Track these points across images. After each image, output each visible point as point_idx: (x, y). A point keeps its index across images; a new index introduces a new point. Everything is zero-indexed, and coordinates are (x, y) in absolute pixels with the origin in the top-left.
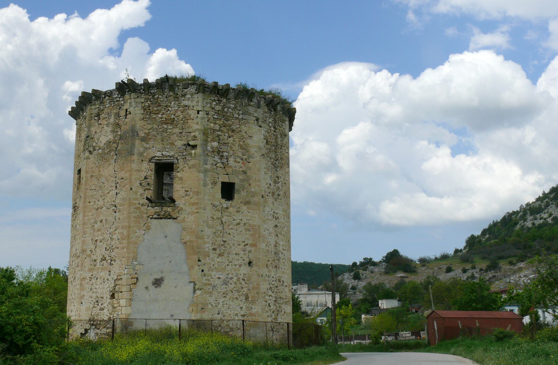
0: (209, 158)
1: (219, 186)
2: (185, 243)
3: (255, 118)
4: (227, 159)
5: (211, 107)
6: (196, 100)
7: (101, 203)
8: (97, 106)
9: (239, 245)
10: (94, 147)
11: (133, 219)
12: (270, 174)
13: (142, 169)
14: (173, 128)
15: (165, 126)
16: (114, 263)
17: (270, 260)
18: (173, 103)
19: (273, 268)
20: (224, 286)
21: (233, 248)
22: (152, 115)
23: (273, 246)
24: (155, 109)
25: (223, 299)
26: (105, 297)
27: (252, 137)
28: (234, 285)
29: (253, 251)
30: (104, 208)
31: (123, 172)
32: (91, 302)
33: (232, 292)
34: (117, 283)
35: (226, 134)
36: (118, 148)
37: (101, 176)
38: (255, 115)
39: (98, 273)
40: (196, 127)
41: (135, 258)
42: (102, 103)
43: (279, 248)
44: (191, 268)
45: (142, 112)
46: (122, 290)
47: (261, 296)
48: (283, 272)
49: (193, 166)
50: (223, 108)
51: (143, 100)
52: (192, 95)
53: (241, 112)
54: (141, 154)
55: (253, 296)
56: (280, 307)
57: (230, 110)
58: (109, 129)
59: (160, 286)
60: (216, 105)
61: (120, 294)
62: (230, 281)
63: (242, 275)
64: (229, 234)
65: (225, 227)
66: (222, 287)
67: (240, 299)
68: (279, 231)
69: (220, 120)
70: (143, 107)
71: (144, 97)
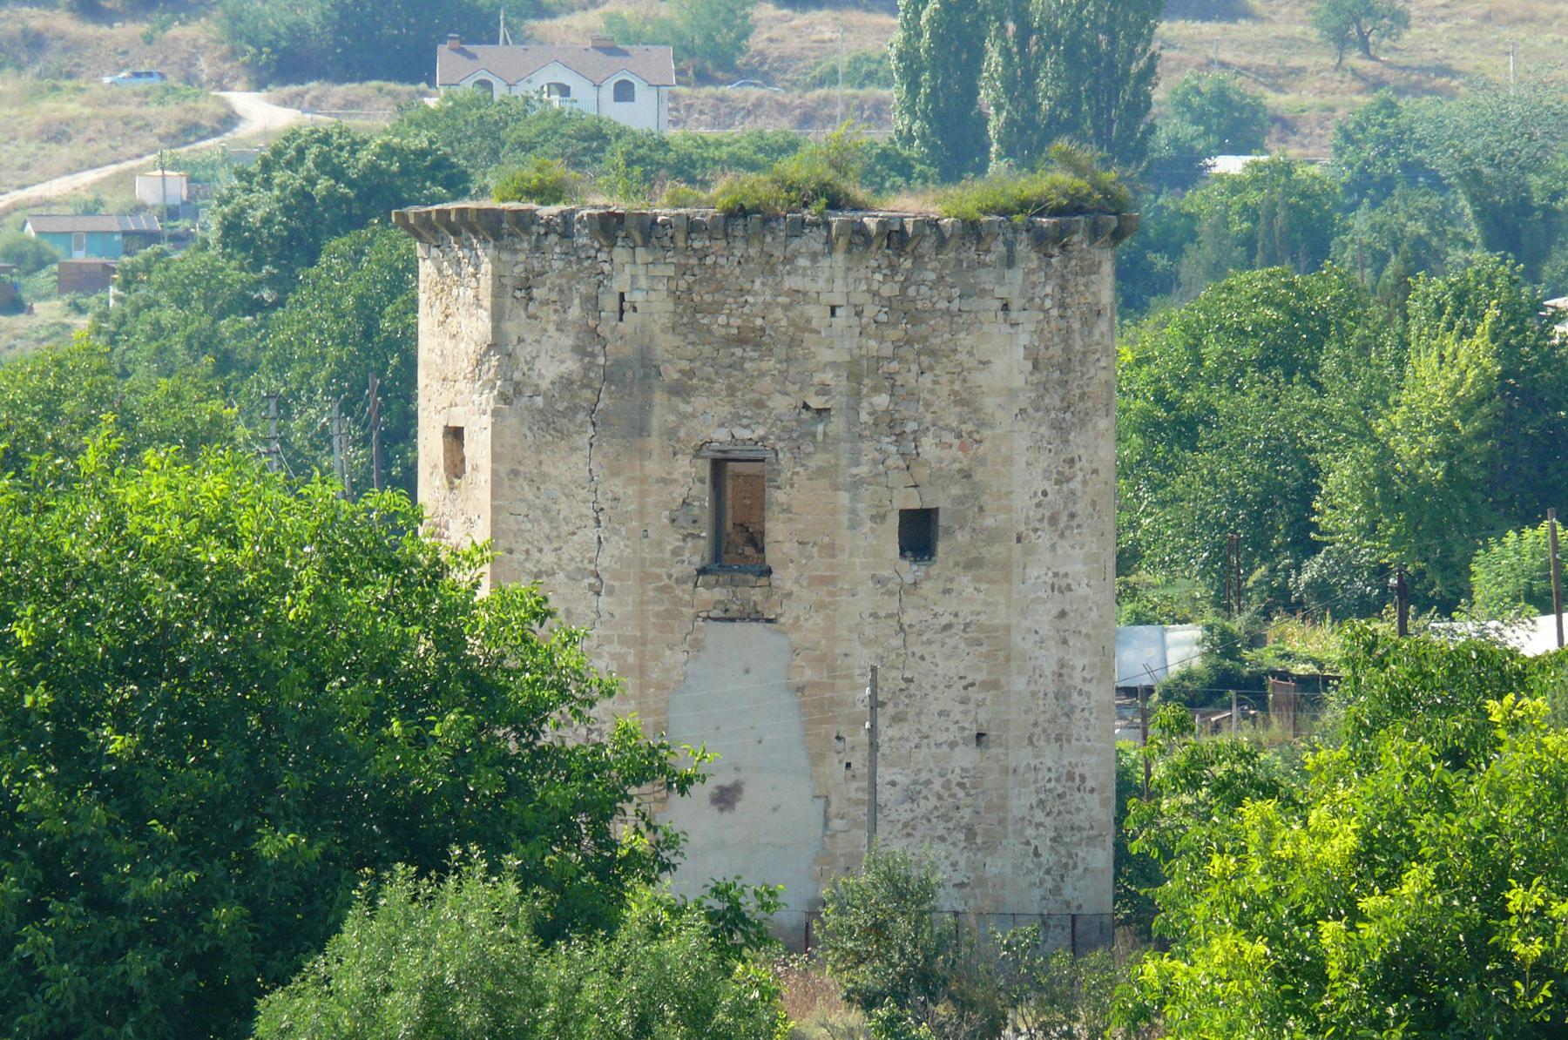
0: (865, 446)
1: (894, 521)
2: (800, 689)
3: (998, 304)
4: (915, 440)
5: (868, 291)
7: (548, 558)
8: (521, 257)
9: (949, 687)
10: (517, 384)
12: (1044, 461)
13: (676, 476)
14: (761, 358)
15: (738, 352)
17: (1042, 718)
19: (1048, 741)
20: (908, 805)
21: (930, 698)
22: (699, 316)
23: (1050, 677)
24: (708, 298)
25: (904, 842)
27: (989, 362)
28: (933, 802)
29: (988, 702)
30: (561, 576)
31: (617, 481)
33: (929, 820)
35: (915, 368)
36: (600, 406)
37: (545, 477)
38: (1000, 291)
40: (826, 355)
43: (1071, 677)
44: (817, 758)
45: (671, 306)
47: (1010, 828)
48: (1084, 750)
49: (821, 472)
50: (904, 289)
51: (670, 271)
52: (814, 257)
53: (956, 292)
54: (671, 433)
55: (986, 832)
56: (1070, 855)
57: (924, 289)
58: (567, 341)
59: (733, 807)
60: (883, 283)
62: (924, 792)
63: (958, 771)
64: (922, 658)
65: (911, 639)
66: (901, 808)
67: (950, 840)
68: (1073, 626)
69: (895, 325)
70: (671, 293)
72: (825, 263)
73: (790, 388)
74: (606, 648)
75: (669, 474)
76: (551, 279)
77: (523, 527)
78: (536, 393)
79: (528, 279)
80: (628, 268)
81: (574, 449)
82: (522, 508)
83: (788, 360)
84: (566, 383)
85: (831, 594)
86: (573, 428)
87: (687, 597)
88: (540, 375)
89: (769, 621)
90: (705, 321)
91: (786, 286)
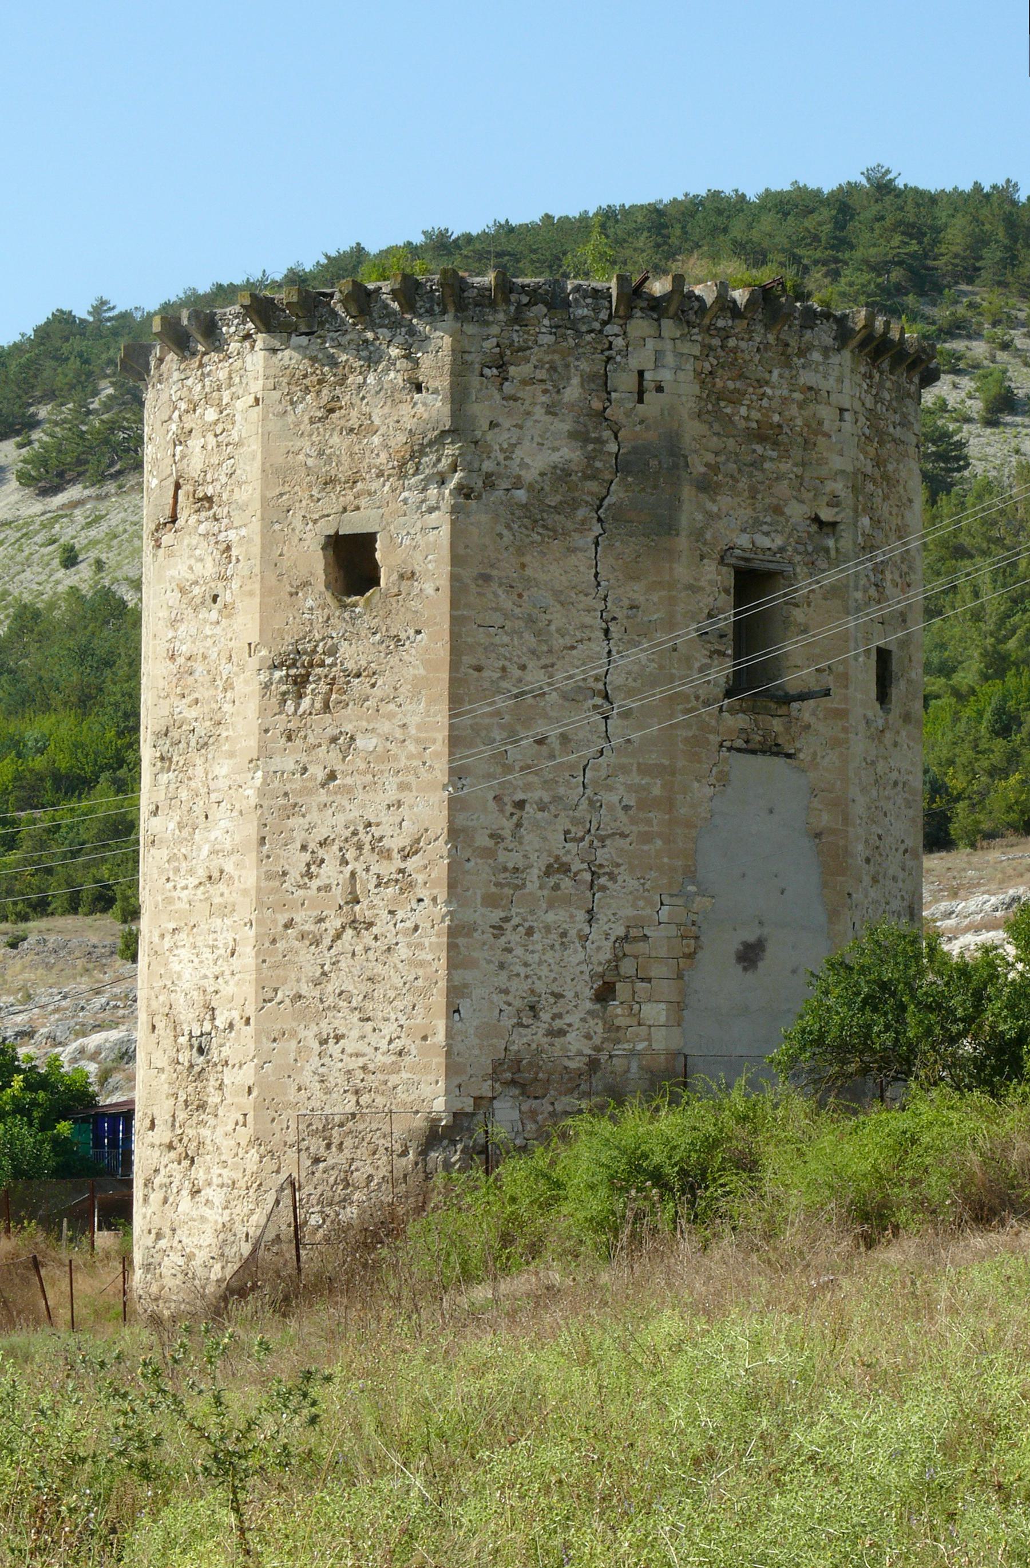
2: (818, 835)
6: (835, 373)
8: (495, 330)
10: (489, 475)
11: (681, 746)
13: (703, 583)
14: (780, 457)
15: (759, 449)
16: (609, 884)
18: (776, 373)
22: (722, 404)
24: (731, 385)
26: (569, 995)
32: (504, 1007)
34: (628, 948)
37: (529, 582)
39: (532, 912)
40: (837, 463)
41: (690, 874)
42: (517, 320)
45: (697, 392)
46: (652, 974)
52: (826, 351)
58: (565, 426)
59: (756, 968)
61: (640, 985)
70: (698, 374)
71: (699, 338)
72: (835, 359)
73: (808, 496)
74: (621, 779)
75: (696, 579)
76: (535, 355)
77: (497, 640)
78: (517, 485)
79: (502, 355)
80: (650, 344)
81: (572, 550)
82: (497, 619)
83: (803, 464)
84: (562, 475)
85: (845, 730)
86: (570, 525)
87: (713, 723)
88: (523, 465)
89: (789, 756)
90: (728, 410)
91: (802, 381)
